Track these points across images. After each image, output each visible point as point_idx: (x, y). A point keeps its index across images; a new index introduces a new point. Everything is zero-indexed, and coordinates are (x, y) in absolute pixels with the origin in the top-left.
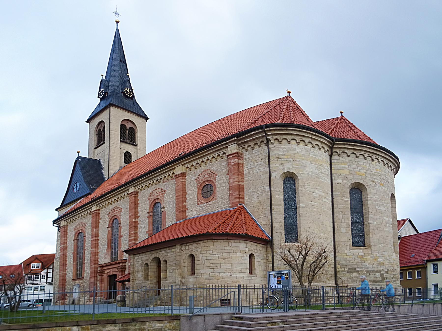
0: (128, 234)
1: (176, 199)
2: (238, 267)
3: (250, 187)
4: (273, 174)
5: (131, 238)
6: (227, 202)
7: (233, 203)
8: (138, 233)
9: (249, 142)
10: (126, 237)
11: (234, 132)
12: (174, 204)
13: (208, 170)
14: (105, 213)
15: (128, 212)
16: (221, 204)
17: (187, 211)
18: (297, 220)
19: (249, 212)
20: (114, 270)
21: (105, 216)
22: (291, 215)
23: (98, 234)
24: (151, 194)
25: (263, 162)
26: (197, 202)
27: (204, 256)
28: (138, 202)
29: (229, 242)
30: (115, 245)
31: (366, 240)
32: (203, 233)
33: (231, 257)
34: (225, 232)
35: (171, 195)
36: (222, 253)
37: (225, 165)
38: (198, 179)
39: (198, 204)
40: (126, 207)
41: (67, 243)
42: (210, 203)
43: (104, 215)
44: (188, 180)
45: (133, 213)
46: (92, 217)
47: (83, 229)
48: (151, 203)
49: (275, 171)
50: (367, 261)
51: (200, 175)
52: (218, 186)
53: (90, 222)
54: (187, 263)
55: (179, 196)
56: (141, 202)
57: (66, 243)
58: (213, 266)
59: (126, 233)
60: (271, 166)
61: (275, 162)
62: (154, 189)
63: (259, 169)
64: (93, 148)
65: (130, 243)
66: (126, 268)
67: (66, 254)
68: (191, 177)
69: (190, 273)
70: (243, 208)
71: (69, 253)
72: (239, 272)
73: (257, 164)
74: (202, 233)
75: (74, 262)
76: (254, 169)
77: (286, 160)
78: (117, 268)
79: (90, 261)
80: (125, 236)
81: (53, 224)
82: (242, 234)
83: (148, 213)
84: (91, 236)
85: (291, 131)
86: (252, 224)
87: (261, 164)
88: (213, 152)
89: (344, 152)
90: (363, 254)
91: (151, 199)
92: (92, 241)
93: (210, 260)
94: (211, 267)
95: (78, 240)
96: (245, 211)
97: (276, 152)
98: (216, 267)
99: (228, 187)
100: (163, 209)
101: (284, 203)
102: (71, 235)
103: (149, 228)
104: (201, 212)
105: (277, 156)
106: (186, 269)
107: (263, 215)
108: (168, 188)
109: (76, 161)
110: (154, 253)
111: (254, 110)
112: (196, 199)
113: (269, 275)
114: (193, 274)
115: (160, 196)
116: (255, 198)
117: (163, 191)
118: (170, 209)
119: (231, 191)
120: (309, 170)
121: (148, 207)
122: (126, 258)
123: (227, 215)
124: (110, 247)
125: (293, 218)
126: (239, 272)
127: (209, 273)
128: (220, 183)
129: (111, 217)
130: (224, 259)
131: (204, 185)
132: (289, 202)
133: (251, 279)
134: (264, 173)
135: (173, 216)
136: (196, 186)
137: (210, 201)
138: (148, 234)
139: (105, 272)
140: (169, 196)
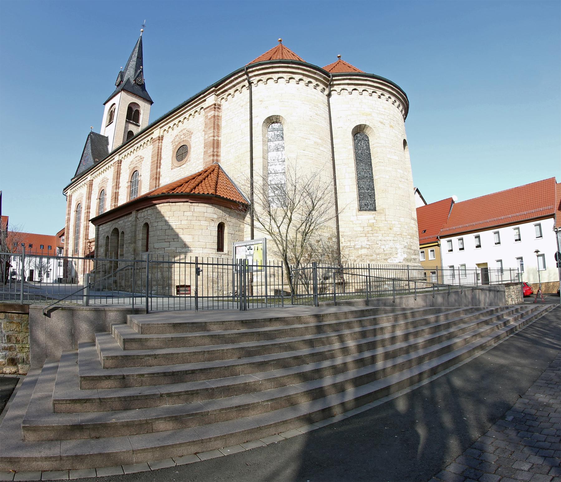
13: (184, 129)
23: (90, 206)
31: (376, 201)
36: (181, 221)
42: (183, 166)
49: (257, 116)
50: (380, 230)
51: (176, 136)
58: (169, 238)
70: (217, 166)
72: (203, 248)
89: (343, 89)
90: (374, 221)
93: (166, 229)
98: (173, 240)
126: (203, 248)
127: (164, 248)
130: (182, 229)
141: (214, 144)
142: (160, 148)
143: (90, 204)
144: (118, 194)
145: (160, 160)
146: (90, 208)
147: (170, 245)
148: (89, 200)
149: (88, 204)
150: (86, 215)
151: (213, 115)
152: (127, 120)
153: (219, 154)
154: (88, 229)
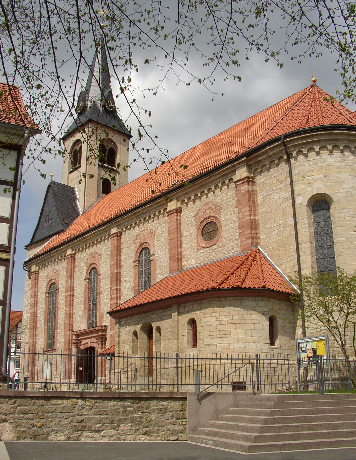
0: (109, 290)
1: (169, 243)
2: (254, 335)
3: (267, 221)
4: (298, 200)
5: (113, 296)
6: (236, 244)
7: (244, 246)
8: (122, 289)
9: (264, 161)
10: (107, 294)
11: (242, 149)
12: (167, 250)
14: (82, 259)
15: (110, 260)
16: (229, 248)
17: (183, 260)
18: (335, 261)
19: (268, 257)
20: (92, 341)
21: (82, 263)
22: (327, 255)
23: (73, 287)
24: (137, 236)
25: (283, 185)
26: (196, 247)
27: (208, 321)
28: (122, 247)
29: (241, 300)
30: (94, 304)
32: (207, 289)
33: (244, 321)
34: (235, 287)
35: (163, 238)
37: (233, 194)
38: (198, 215)
39: (198, 250)
40: (107, 253)
41: (38, 296)
42: (213, 247)
43: (80, 262)
44: (184, 218)
45: (115, 261)
46: (67, 264)
47: (56, 278)
48: (137, 248)
49: (300, 195)
51: (199, 210)
52: (223, 223)
53: (64, 270)
54: (186, 330)
55: (173, 239)
56: (124, 247)
57: (37, 295)
58: (220, 334)
59: (106, 289)
60: (295, 189)
61: (300, 182)
62: (142, 230)
63: (278, 195)
64: (67, 172)
65: (112, 302)
66: (106, 339)
67: (36, 312)
68: (188, 213)
69: (191, 344)
70: (258, 251)
71: (40, 311)
73: (274, 188)
74: (205, 289)
75: (45, 326)
76: (271, 196)
77: (314, 177)
78: (97, 338)
79: (64, 325)
80: (106, 293)
81: (24, 266)
82: (259, 287)
83: (134, 261)
84: (65, 289)
85: (319, 136)
86: (271, 274)
87: (280, 188)
88: (216, 179)
91: (138, 242)
92: (66, 296)
94: (218, 336)
95: (49, 293)
96: (261, 256)
97: (300, 168)
98: (225, 336)
99: (237, 224)
100: (153, 257)
101: (316, 238)
102: (42, 286)
103: (135, 282)
104: (202, 260)
105: (302, 173)
106: (185, 340)
107: (287, 259)
108: (158, 229)
109: (49, 187)
110: (144, 317)
111: (269, 112)
112: (194, 243)
113: (297, 343)
114: (195, 346)
115: (148, 239)
116: (274, 236)
117: (152, 233)
118: (162, 256)
119: (242, 228)
120: (348, 186)
121: (133, 254)
122: (106, 325)
123: (237, 263)
124: (87, 307)
125: (330, 260)
128: (227, 220)
129: (89, 265)
131: (205, 224)
132: (322, 237)
133: (273, 352)
134: (286, 200)
135: (165, 266)
136: (194, 225)
137: (213, 245)
138: (133, 291)
139: (81, 342)
140: (160, 239)
141: (251, 224)
142: (179, 223)
143: (73, 285)
144: (120, 275)
145: (181, 238)
146: (73, 291)
147: (222, 340)
148: (71, 279)
149: (71, 285)
150: (69, 299)
151: (247, 190)
152: (100, 163)
153: (258, 236)
154: (73, 318)
